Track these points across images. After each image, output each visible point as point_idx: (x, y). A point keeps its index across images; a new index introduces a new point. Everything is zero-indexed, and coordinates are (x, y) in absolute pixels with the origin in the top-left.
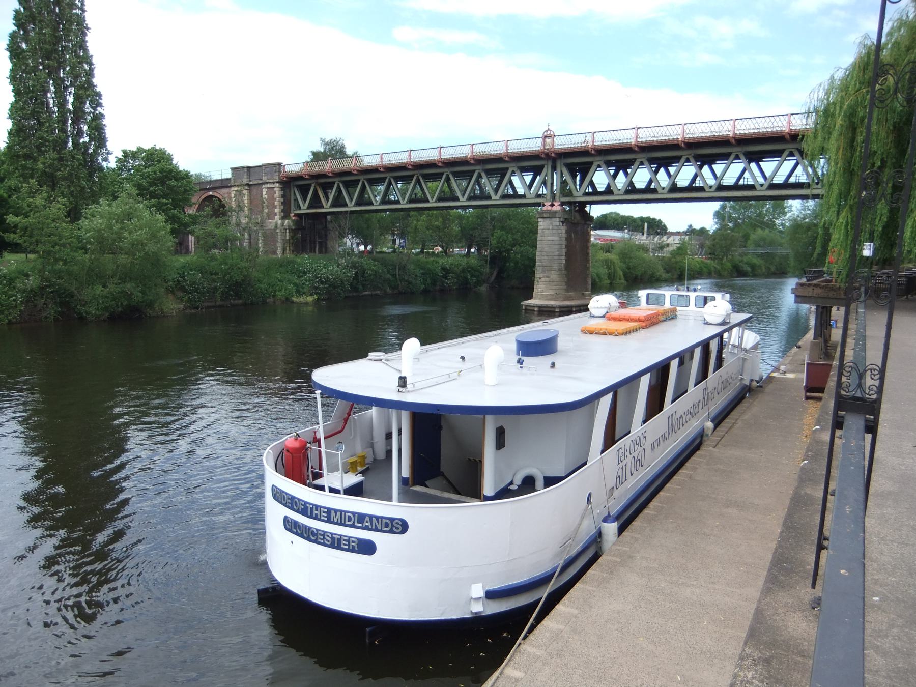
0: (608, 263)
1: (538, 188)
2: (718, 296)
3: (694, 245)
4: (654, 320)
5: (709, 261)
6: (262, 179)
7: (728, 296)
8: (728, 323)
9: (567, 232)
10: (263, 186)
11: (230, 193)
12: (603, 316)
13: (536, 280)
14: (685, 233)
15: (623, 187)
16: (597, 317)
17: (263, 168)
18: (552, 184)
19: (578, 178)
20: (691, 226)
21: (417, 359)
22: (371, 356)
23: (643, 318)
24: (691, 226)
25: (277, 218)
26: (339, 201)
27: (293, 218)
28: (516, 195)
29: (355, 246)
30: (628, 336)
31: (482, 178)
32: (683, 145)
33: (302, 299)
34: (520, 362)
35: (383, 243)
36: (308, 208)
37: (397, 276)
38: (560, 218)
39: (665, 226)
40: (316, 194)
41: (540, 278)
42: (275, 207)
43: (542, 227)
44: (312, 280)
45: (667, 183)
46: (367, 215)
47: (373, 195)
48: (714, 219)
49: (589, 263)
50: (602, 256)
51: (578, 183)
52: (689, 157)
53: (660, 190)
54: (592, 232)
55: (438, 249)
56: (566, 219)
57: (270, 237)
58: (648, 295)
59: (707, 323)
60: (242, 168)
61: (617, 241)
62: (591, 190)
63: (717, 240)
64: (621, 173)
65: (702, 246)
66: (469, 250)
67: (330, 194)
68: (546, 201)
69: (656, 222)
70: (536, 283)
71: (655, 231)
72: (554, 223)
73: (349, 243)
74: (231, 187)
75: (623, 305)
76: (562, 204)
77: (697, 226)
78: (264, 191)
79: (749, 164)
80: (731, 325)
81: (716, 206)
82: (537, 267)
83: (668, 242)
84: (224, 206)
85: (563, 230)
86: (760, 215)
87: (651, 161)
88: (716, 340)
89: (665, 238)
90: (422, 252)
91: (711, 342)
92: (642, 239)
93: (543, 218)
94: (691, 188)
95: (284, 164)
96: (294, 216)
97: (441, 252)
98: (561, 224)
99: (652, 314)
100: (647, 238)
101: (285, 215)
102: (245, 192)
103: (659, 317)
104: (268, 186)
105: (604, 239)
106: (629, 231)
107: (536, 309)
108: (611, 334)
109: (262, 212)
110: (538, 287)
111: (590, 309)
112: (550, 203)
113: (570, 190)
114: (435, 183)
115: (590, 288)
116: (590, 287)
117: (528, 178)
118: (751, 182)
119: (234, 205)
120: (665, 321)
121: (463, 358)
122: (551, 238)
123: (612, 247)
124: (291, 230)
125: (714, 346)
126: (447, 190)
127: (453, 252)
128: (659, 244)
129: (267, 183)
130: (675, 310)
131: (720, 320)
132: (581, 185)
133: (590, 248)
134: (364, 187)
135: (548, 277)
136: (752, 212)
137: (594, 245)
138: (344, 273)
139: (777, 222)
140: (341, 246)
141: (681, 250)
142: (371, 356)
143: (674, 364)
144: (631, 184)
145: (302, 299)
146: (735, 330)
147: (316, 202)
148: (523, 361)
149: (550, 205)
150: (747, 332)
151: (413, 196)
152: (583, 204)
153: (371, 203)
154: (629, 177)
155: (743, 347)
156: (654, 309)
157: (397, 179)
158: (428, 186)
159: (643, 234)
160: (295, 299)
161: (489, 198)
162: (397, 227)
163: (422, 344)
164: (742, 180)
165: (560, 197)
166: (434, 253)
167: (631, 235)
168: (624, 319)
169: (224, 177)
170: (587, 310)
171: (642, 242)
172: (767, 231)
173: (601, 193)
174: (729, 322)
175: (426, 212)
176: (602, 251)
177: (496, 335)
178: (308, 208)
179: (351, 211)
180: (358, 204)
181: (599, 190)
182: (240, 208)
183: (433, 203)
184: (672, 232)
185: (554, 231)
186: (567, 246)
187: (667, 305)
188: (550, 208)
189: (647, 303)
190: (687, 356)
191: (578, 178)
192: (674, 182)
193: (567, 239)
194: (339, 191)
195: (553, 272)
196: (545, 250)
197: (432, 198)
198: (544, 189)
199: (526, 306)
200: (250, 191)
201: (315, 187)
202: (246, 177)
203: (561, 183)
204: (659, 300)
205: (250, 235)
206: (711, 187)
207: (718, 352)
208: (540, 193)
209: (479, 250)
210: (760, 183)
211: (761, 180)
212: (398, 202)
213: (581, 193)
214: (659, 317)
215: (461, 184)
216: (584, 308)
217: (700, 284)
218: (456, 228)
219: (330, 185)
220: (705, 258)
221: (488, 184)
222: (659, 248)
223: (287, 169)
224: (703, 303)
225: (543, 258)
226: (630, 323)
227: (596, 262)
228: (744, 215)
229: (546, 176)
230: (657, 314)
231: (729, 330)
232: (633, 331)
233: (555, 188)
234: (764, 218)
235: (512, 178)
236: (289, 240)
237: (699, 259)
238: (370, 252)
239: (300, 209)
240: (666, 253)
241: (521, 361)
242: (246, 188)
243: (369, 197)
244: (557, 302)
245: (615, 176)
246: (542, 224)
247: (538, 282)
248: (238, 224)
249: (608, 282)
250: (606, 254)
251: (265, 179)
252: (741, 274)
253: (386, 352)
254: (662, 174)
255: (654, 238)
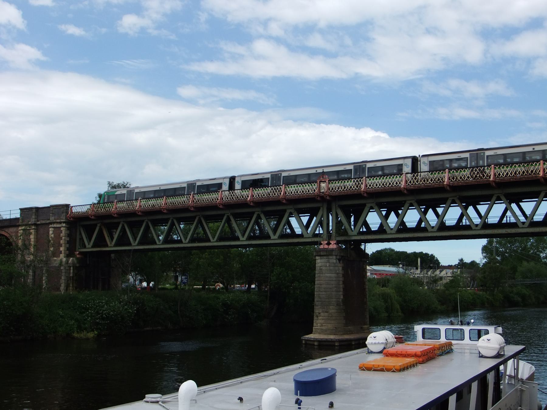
0: (385, 297)
1: (315, 227)
2: (491, 329)
3: (467, 278)
4: (431, 355)
5: (481, 293)
6: (49, 219)
7: (500, 329)
8: (504, 355)
9: (343, 269)
10: (50, 226)
11: (18, 232)
12: (381, 352)
13: (315, 315)
14: (456, 267)
15: (395, 226)
16: (374, 353)
17: (51, 208)
18: (328, 224)
19: (352, 219)
20: (461, 260)
21: (194, 401)
22: (148, 398)
23: (420, 354)
24: (461, 260)
25: (62, 256)
26: (123, 240)
27: (78, 256)
28: (293, 234)
29: (137, 282)
30: (406, 372)
31: (261, 219)
32: (448, 188)
33: (83, 335)
34: (298, 402)
35: (166, 279)
36: (93, 247)
37: (179, 312)
38: (336, 256)
39: (437, 260)
40: (101, 233)
41: (319, 313)
42: (61, 246)
43: (320, 265)
44: (94, 316)
45: (436, 223)
46: (150, 253)
47: (156, 235)
48: (482, 253)
49: (367, 298)
50: (379, 290)
51: (352, 223)
52: (455, 198)
53: (429, 229)
54: (368, 268)
55: (219, 286)
56: (342, 256)
57: (53, 274)
58: (424, 330)
59: (482, 356)
60: (31, 209)
61: (393, 275)
62: (365, 230)
63: (487, 273)
64: (393, 214)
65: (473, 279)
66: (249, 286)
67: (114, 233)
68: (323, 240)
69: (429, 257)
70: (315, 318)
71: (427, 266)
72: (331, 261)
73: (131, 280)
74: (19, 226)
75: (399, 340)
76: (338, 243)
77: (467, 260)
78: (51, 231)
79: (510, 204)
80: (506, 357)
81: (484, 242)
82: (316, 303)
83: (440, 275)
84: (10, 244)
85: (340, 268)
86: (525, 249)
87: (420, 203)
88: (492, 373)
89: (438, 272)
90: (204, 288)
91: (488, 375)
92: (417, 273)
93: (320, 256)
94: (458, 226)
95: (71, 205)
96: (78, 254)
97: (222, 288)
98: (338, 261)
99: (428, 349)
100: (421, 272)
101: (70, 253)
102: (31, 231)
103: (436, 352)
104: (55, 225)
105: (380, 274)
106: (403, 265)
107: (316, 343)
108: (388, 370)
109: (47, 251)
110: (318, 321)
111: (368, 345)
112: (326, 242)
113: (345, 230)
114: (216, 224)
115: (368, 323)
116: (368, 320)
117: (305, 219)
118: (513, 220)
119: (20, 243)
120: (441, 355)
121: (241, 399)
122: (328, 275)
123: (388, 280)
124: (75, 268)
125: (491, 378)
126: (227, 229)
127: (234, 288)
128: (433, 277)
129: (54, 223)
130: (450, 344)
131: (494, 353)
132: (355, 225)
133: (367, 283)
134: (147, 227)
135: (327, 312)
136: (517, 246)
137: (370, 280)
138: (126, 309)
139: (541, 255)
140: (125, 282)
141: (454, 282)
142: (148, 398)
143: (453, 399)
144: (403, 223)
145: (83, 335)
146: (510, 363)
147: (100, 241)
148: (301, 401)
149: (326, 244)
150: (522, 363)
151: (195, 235)
152: (358, 243)
153: (155, 243)
154: (400, 217)
155: (519, 377)
156: (431, 343)
157: (180, 220)
158: (209, 226)
159: (417, 269)
160: (75, 335)
161: (268, 237)
162: (179, 264)
163: (199, 385)
164: (505, 219)
165: (336, 236)
166: (215, 288)
167: (406, 270)
168: (401, 355)
169: (13, 216)
170: (365, 346)
171: (416, 276)
172: (532, 264)
173: (375, 232)
174: (504, 355)
175: (208, 250)
176: (378, 286)
177: (274, 374)
178: (93, 247)
179: (134, 250)
180: (141, 243)
181: (372, 230)
182: (26, 246)
183: (213, 243)
184: (444, 266)
185: (332, 268)
186: (344, 282)
187: (443, 340)
188: (326, 246)
189: (423, 337)
190: (465, 391)
191: (352, 219)
192: (442, 221)
193: (344, 275)
194: (123, 231)
195: (331, 307)
196: (324, 286)
197: (214, 238)
198: (321, 229)
199: (306, 340)
200: (37, 230)
201: (100, 226)
202: (33, 217)
203: (336, 223)
204: (436, 334)
205: (34, 272)
206: (477, 225)
207: (495, 383)
208: (317, 232)
209: (259, 286)
210: (522, 221)
211: (522, 219)
212: (180, 242)
213: (355, 233)
214: (436, 352)
215: (241, 224)
216: (361, 344)
217: (473, 315)
218: (236, 266)
219: (116, 226)
220: (478, 290)
221: (268, 225)
222: (432, 281)
223: (74, 210)
224: (477, 336)
225: (321, 293)
226: (407, 359)
227: (373, 296)
228: (510, 250)
229: (322, 217)
230: (433, 349)
231: (505, 362)
232: (410, 367)
233: (331, 228)
234: (530, 251)
235: (290, 218)
236: (73, 277)
237: (470, 291)
238: (152, 289)
239: (85, 247)
240: (439, 286)
241: (299, 401)
242: (33, 227)
243: (153, 237)
244: (336, 336)
245: (387, 216)
246: (320, 262)
247: (317, 316)
248: (23, 262)
249: (386, 314)
250: (383, 289)
251: (52, 219)
252: (513, 304)
253: (163, 394)
254: (431, 216)
255: (427, 272)
